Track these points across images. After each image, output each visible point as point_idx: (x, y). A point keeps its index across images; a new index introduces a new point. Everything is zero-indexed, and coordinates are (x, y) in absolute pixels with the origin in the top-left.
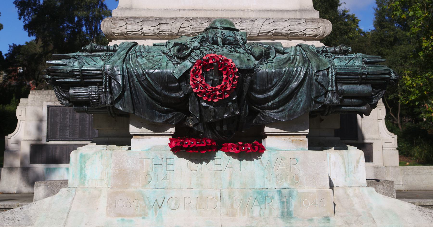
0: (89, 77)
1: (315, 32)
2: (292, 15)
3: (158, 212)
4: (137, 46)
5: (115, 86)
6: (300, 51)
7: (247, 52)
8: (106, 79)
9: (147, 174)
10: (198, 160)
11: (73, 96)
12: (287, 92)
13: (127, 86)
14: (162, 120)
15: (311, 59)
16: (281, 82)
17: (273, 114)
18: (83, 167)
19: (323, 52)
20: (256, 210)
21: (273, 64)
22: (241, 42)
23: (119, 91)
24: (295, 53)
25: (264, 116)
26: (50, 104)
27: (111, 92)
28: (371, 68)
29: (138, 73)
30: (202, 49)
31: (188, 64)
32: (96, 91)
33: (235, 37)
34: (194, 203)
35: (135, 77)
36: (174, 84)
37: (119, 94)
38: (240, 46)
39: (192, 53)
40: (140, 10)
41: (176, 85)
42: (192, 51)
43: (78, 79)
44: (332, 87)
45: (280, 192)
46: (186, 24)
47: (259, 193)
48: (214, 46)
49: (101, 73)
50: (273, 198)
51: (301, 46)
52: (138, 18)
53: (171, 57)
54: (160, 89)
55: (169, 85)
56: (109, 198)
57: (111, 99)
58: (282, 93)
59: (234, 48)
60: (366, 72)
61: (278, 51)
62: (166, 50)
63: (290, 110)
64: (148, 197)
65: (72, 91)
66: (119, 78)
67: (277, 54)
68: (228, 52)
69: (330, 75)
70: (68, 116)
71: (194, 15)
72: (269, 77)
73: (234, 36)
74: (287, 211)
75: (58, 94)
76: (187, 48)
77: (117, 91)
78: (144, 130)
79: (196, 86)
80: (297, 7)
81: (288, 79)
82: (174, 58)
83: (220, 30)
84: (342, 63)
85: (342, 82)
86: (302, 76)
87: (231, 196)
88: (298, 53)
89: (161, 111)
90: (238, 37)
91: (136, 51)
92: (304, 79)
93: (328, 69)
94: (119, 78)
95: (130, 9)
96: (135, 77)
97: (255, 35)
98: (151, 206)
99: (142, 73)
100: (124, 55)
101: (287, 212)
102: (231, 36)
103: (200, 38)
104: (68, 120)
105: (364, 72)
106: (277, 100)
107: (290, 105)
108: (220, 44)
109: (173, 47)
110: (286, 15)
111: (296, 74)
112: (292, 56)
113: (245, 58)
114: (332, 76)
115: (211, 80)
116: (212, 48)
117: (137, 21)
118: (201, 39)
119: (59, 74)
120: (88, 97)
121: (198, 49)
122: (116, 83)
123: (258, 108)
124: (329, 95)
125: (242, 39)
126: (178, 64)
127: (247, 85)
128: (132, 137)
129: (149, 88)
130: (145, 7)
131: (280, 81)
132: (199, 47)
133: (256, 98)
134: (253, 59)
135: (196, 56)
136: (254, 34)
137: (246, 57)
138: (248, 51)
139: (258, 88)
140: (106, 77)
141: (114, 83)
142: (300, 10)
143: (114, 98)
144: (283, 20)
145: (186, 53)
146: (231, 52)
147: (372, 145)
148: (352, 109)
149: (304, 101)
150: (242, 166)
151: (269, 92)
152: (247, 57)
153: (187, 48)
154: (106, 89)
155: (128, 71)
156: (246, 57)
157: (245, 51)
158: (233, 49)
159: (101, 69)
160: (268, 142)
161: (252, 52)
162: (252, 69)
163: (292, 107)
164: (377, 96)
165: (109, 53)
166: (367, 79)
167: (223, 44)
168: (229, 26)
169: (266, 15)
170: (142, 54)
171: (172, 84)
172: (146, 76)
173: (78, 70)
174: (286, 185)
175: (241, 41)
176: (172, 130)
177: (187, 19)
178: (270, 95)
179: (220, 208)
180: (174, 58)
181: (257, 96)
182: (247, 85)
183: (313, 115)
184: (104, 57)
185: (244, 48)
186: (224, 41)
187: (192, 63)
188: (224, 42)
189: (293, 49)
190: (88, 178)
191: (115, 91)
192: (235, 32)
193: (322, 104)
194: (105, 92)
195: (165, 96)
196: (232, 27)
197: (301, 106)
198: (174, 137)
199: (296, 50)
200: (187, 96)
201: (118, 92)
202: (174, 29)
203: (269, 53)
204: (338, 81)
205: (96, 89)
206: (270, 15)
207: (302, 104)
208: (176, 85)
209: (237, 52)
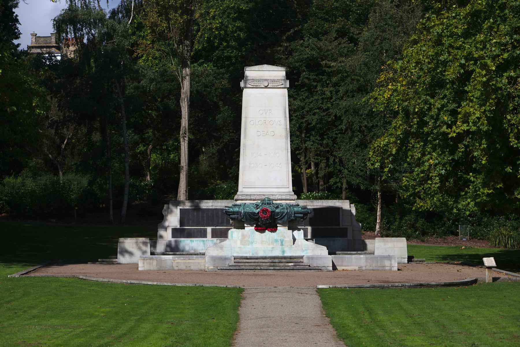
1: (292, 198)
2: (286, 194)
9: (249, 236)
10: (262, 233)
11: (231, 217)
12: (282, 216)
14: (253, 223)
17: (279, 222)
20: (275, 244)
28: (303, 210)
31: (259, 210)
34: (260, 242)
40: (245, 192)
45: (280, 240)
46: (258, 197)
47: (276, 240)
52: (244, 195)
54: (252, 216)
61: (281, 206)
62: (253, 206)
65: (231, 216)
70: (191, 214)
71: (260, 194)
72: (278, 213)
76: (258, 206)
77: (242, 216)
78: (249, 226)
79: (261, 215)
80: (288, 191)
87: (269, 241)
95: (242, 192)
98: (240, 248)
104: (191, 216)
127: (273, 215)
129: (250, 216)
130: (246, 191)
142: (289, 192)
144: (284, 195)
153: (258, 206)
160: (278, 228)
174: (282, 238)
176: (255, 225)
182: (273, 215)
183: (289, 221)
188: (268, 204)
198: (255, 227)
200: (258, 218)
204: (295, 214)
206: (280, 194)
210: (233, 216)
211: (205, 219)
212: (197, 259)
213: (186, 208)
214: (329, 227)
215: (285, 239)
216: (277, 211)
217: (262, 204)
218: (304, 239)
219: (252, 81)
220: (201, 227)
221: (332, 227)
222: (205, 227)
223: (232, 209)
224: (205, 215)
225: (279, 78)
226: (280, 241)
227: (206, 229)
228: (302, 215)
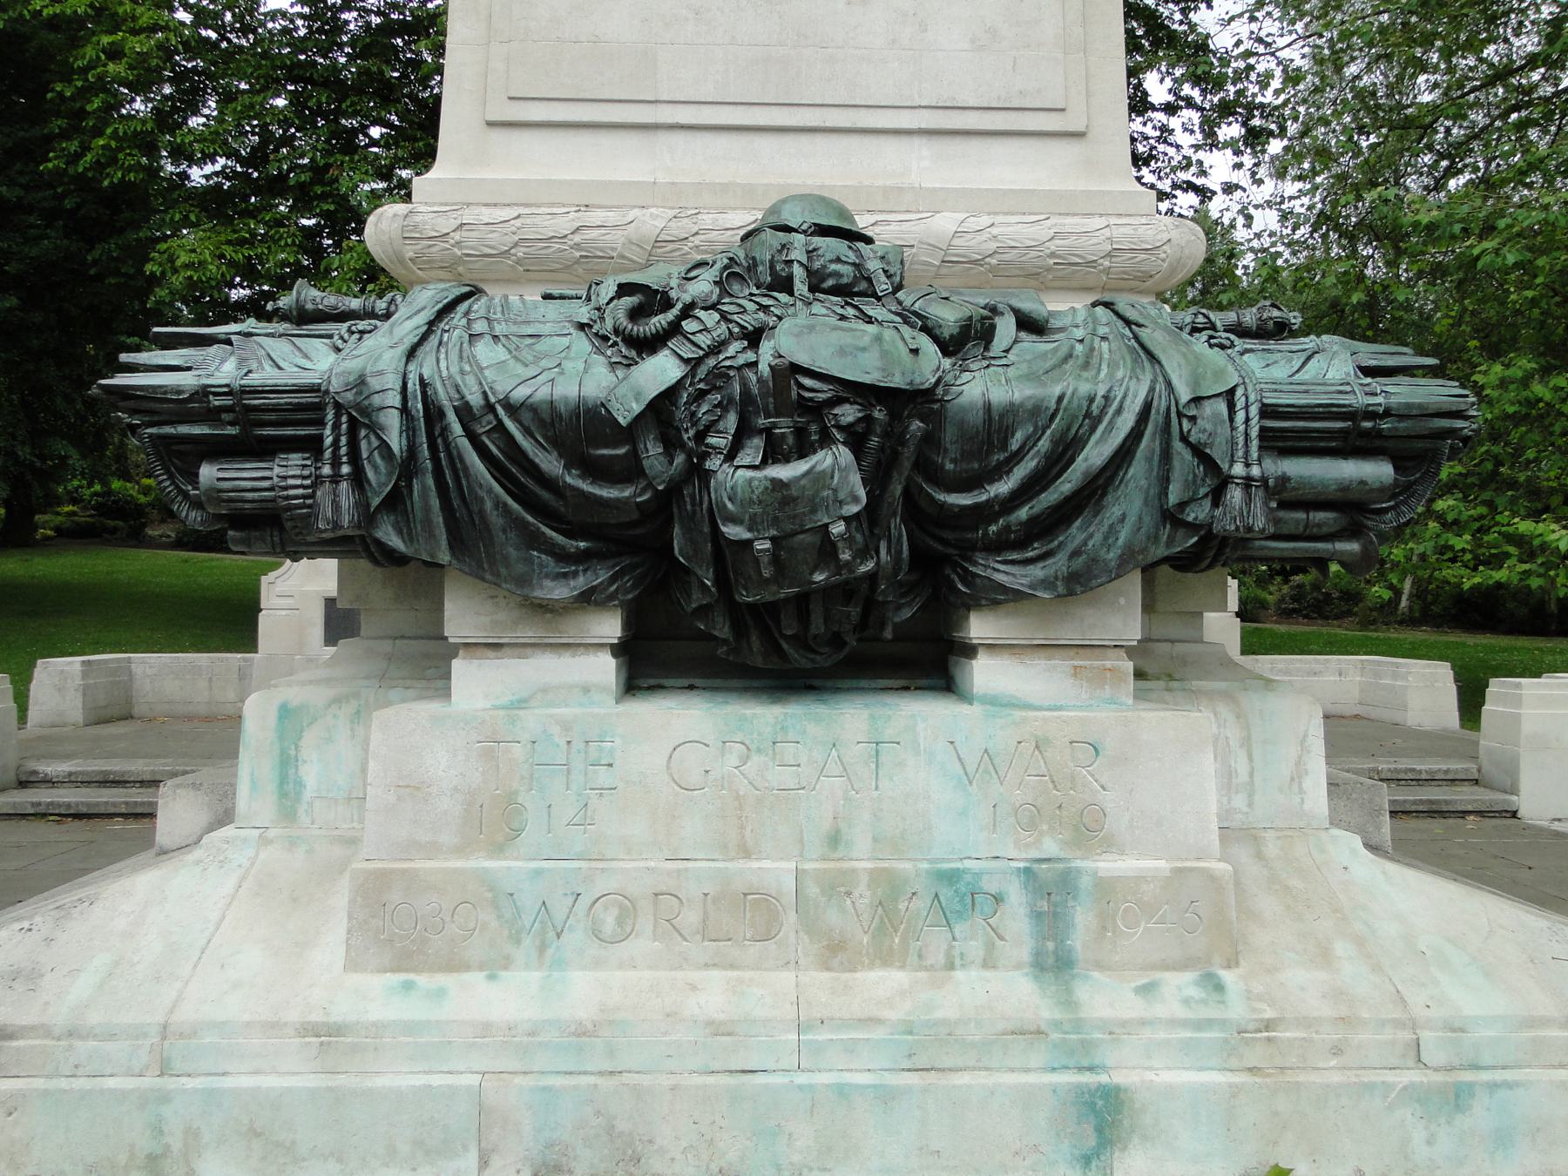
0: (273, 417)
3: (550, 952)
4: (477, 300)
5: (371, 453)
7: (906, 321)
8: (336, 426)
11: (215, 495)
12: (1066, 484)
13: (420, 455)
16: (1044, 444)
18: (292, 752)
22: (883, 285)
23: (390, 474)
25: (969, 578)
27: (358, 479)
29: (467, 403)
30: (725, 308)
32: (306, 472)
35: (451, 417)
36: (615, 448)
37: (389, 488)
38: (879, 299)
39: (683, 323)
41: (621, 451)
42: (688, 311)
43: (232, 424)
44: (1247, 465)
48: (775, 294)
49: (317, 400)
50: (998, 899)
51: (1112, 304)
53: (605, 338)
54: (550, 463)
55: (592, 452)
56: (359, 899)
57: (362, 504)
58: (1044, 489)
59: (856, 307)
60: (1380, 405)
63: (1076, 553)
64: (511, 895)
66: (392, 423)
67: (1023, 335)
73: (852, 257)
74: (1056, 948)
75: (168, 483)
76: (667, 304)
81: (1073, 431)
82: (615, 344)
83: (801, 237)
85: (1280, 444)
86: (1127, 422)
89: (562, 556)
91: (472, 316)
92: (1135, 435)
93: (1232, 392)
94: (392, 423)
96: (451, 417)
97: (927, 271)
99: (482, 402)
100: (417, 332)
101: (1055, 952)
102: (844, 259)
103: (718, 266)
105: (1371, 408)
106: (1023, 513)
107: (1075, 534)
108: (801, 287)
109: (612, 300)
111: (1103, 411)
112: (1081, 341)
113: (901, 344)
114: (1247, 420)
115: (760, 431)
116: (766, 301)
118: (726, 268)
119: (157, 406)
120: (273, 500)
121: (713, 307)
122: (375, 443)
124: (1235, 495)
125: (885, 271)
126: (630, 365)
128: (455, 656)
131: (1039, 439)
132: (714, 297)
133: (942, 506)
134: (925, 343)
135: (700, 331)
136: (923, 271)
137: (903, 339)
138: (914, 319)
139: (949, 466)
140: (338, 416)
141: (369, 443)
143: (368, 505)
145: (659, 321)
146: (843, 318)
148: (1306, 550)
149: (1132, 519)
150: (880, 773)
151: (992, 481)
152: (909, 341)
153: (667, 304)
154: (336, 463)
155: (424, 393)
156: (903, 339)
157: (898, 319)
159: (320, 385)
160: (983, 673)
161: (930, 324)
162: (927, 390)
163: (1085, 543)
164: (1404, 502)
166: (1377, 434)
167: (812, 289)
168: (834, 223)
170: (492, 328)
171: (606, 446)
172: (496, 416)
173: (226, 390)
174: (1050, 847)
175: (883, 278)
178: (996, 496)
179: (792, 935)
180: (615, 344)
181: (942, 497)
184: (342, 338)
185: (893, 309)
186: (814, 281)
187: (687, 361)
190: (308, 794)
191: (370, 474)
192: (861, 245)
193: (1202, 533)
194: (336, 478)
196: (846, 226)
197: (1121, 542)
201: (383, 479)
202: (634, 247)
203: (993, 327)
205: (304, 466)
207: (1123, 535)
208: (621, 451)
215: (1109, 865)
226: (1016, 897)
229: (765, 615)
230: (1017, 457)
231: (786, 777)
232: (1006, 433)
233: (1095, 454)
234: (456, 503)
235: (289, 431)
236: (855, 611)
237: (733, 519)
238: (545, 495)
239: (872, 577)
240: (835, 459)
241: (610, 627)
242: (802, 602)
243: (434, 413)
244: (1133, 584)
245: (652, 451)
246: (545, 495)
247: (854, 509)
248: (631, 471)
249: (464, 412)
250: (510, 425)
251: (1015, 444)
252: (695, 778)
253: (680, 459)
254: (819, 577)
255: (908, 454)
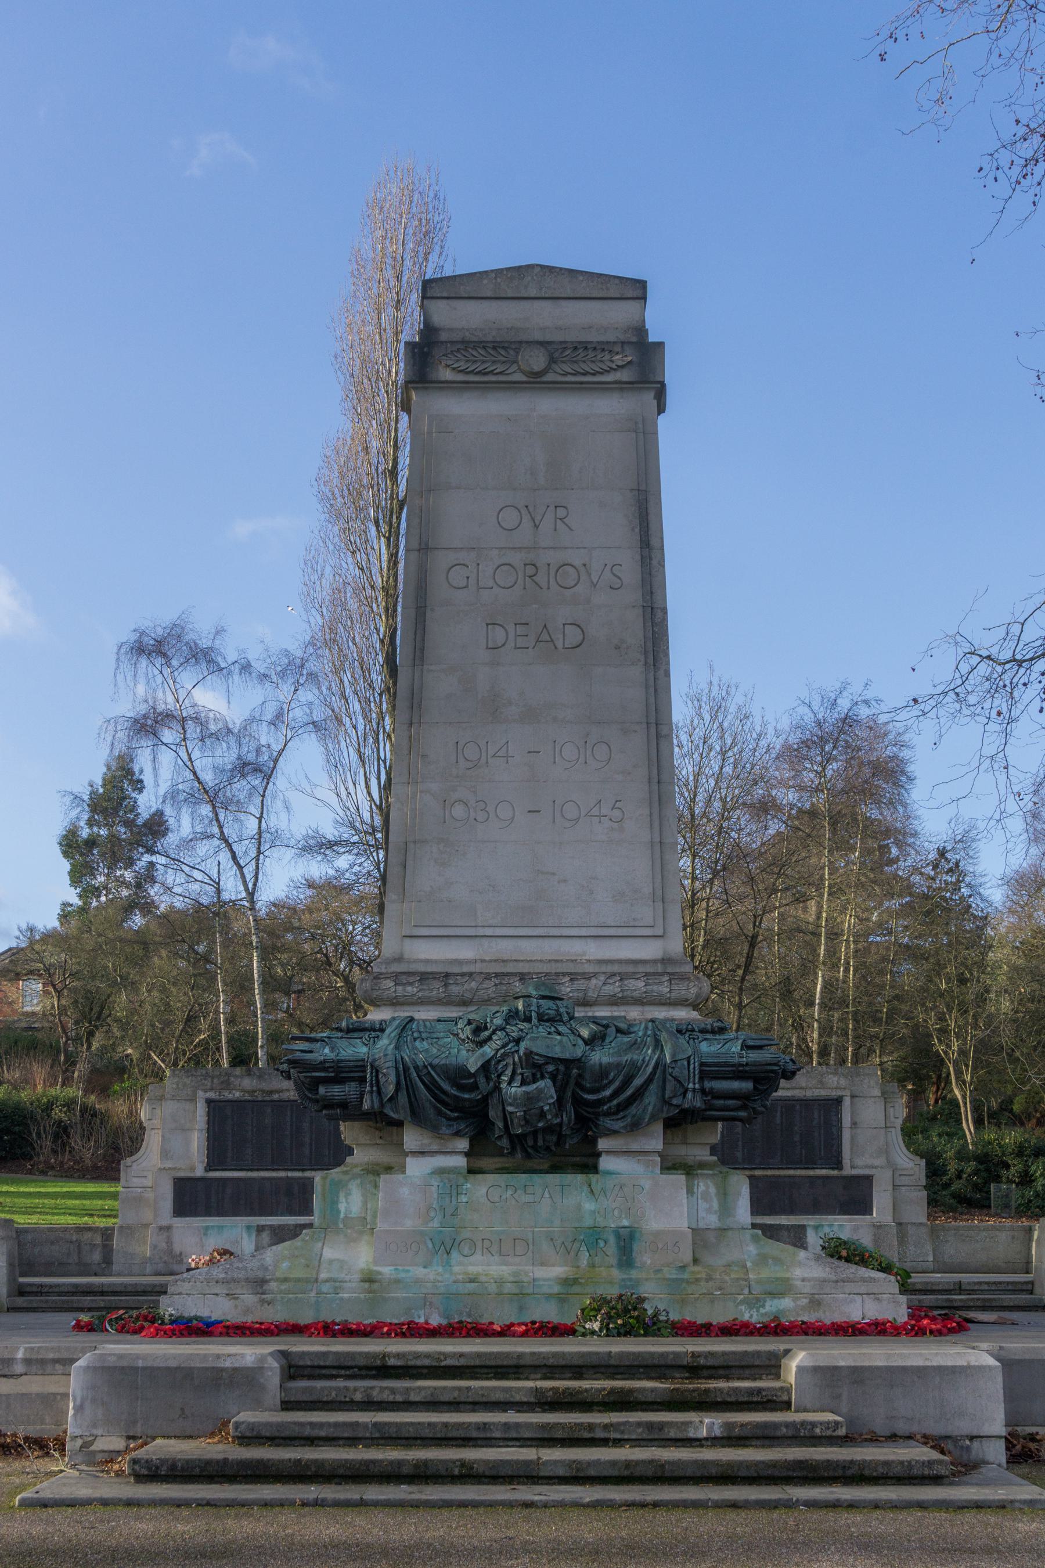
2: (649, 969)
6: (653, 1029)
12: (629, 1092)
15: (666, 1042)
16: (621, 1078)
17: (608, 1123)
19: (687, 1030)
21: (611, 1051)
22: (566, 1018)
24: (645, 1035)
26: (211, 1095)
28: (754, 1056)
33: (557, 1011)
42: (494, 1032)
54: (446, 1086)
61: (619, 1031)
63: (634, 1116)
65: (322, 1090)
68: (545, 1034)
69: (692, 1067)
72: (603, 1072)
84: (712, 1049)
86: (650, 1069)
88: (649, 1032)
89: (449, 1119)
90: (561, 1010)
96: (412, 1070)
106: (615, 1102)
107: (633, 1110)
108: (534, 1021)
110: (641, 969)
117: (411, 979)
123: (588, 1113)
124: (690, 1095)
129: (433, 1088)
133: (582, 1098)
134: (580, 1042)
139: (588, 1085)
146: (549, 1033)
147: (872, 1180)
149: (652, 1104)
153: (486, 1029)
158: (553, 1029)
160: (606, 1163)
165: (373, 1034)
168: (548, 994)
169: (610, 969)
174: (626, 1223)
177: (488, 977)
181: (586, 1096)
188: (541, 1018)
189: (643, 1026)
192: (558, 1002)
195: (456, 1097)
199: (646, 1028)
204: (704, 1076)
206: (616, 968)
209: (559, 1034)
210: (336, 1091)
211: (307, 1140)
212: (34, 1369)
213: (230, 1096)
214: (799, 1172)
216: (599, 1057)
217: (507, 1021)
218: (754, 1226)
219: (459, 346)
220: (290, 1174)
221: (811, 1173)
222: (308, 1174)
223: (332, 1050)
224: (306, 1125)
225: (611, 337)
226: (612, 1240)
227: (311, 1180)
228: (747, 1086)
229: (522, 1137)
230: (611, 1082)
231: (529, 1198)
232: (607, 1075)
233: (638, 1082)
234: (413, 1100)
235: (352, 1075)
236: (554, 1138)
237: (511, 1105)
238: (444, 1097)
239: (560, 1125)
240: (545, 1085)
241: (463, 1144)
242: (535, 1133)
243: (406, 1069)
244: (659, 1127)
245: (481, 1081)
246: (444, 1097)
247: (552, 1101)
248: (474, 1087)
249: (416, 1068)
250: (433, 1073)
251: (611, 1078)
252: (497, 1199)
253: (491, 1084)
254: (540, 1125)
255: (572, 1081)
